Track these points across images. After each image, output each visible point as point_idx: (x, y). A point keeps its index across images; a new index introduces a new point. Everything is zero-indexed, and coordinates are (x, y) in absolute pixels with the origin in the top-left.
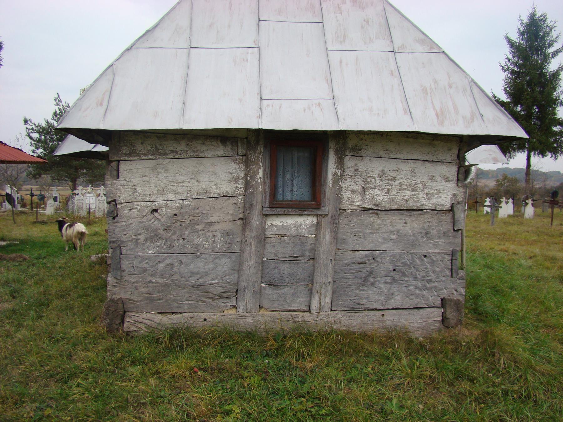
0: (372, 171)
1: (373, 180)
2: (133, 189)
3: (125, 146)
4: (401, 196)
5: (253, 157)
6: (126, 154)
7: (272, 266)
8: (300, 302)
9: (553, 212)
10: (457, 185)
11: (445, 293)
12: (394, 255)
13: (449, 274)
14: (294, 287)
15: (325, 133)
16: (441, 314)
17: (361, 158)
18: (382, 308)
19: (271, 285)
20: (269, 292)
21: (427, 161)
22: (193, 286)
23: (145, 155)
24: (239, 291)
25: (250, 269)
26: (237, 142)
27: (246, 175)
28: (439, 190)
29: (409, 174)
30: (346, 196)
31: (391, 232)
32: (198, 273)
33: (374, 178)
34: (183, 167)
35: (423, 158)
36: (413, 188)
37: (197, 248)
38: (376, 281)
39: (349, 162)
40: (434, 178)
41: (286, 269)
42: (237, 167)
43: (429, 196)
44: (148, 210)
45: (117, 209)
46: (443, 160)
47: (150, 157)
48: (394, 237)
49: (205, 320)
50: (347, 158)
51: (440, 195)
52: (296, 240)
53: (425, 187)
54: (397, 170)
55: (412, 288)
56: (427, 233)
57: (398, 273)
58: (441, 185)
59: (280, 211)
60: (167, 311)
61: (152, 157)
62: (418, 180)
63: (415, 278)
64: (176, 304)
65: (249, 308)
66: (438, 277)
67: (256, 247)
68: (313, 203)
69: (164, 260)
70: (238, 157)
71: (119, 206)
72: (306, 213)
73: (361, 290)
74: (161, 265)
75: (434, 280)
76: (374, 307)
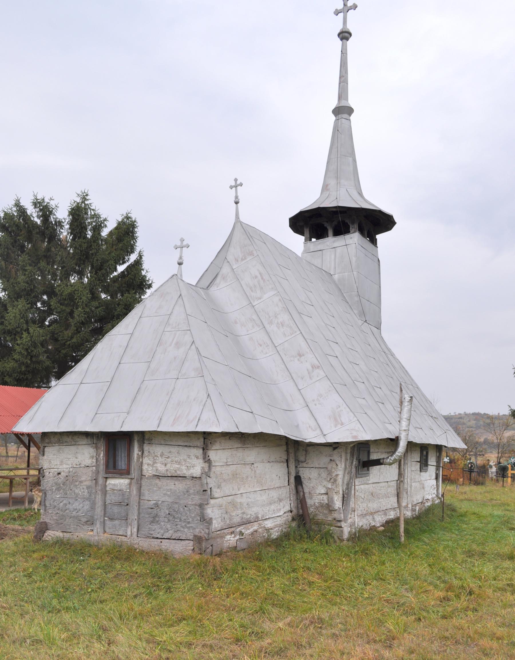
2: (50, 462)
4: (172, 468)
5: (99, 445)
7: (110, 507)
11: (197, 532)
12: (168, 505)
15: (429, 445)
20: (108, 523)
21: (186, 446)
22: (74, 517)
23: (55, 443)
25: (99, 510)
29: (177, 454)
30: (145, 467)
31: (167, 490)
32: (76, 509)
36: (179, 463)
37: (77, 495)
39: (146, 447)
44: (56, 473)
48: (169, 493)
52: (120, 492)
54: (170, 452)
55: (179, 526)
56: (187, 492)
57: (171, 516)
58: (195, 461)
62: (182, 458)
64: (68, 527)
66: (193, 520)
69: (63, 501)
72: (123, 477)
74: (62, 504)
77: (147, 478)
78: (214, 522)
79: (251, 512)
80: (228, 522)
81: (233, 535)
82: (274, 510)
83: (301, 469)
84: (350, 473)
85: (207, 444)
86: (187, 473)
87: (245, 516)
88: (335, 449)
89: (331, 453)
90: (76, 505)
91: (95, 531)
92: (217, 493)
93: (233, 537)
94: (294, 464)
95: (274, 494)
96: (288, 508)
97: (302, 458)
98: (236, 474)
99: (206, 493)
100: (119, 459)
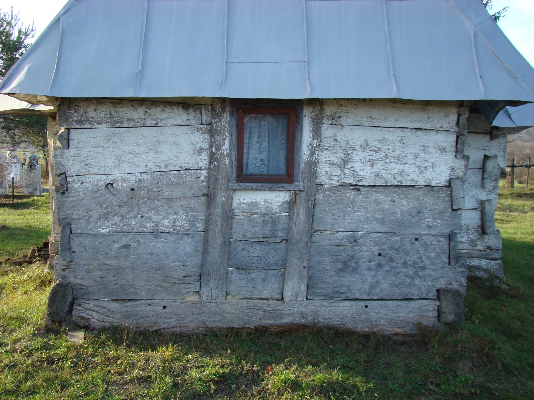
0: (353, 142)
1: (355, 152)
3: (76, 112)
4: (389, 172)
6: (77, 122)
7: (241, 247)
8: (270, 289)
10: (456, 157)
11: (441, 284)
12: (379, 238)
13: (447, 260)
14: (265, 271)
16: (437, 308)
17: (340, 126)
18: (366, 298)
19: (239, 269)
23: (100, 123)
24: (202, 275)
26: (201, 110)
27: (211, 146)
28: (433, 163)
30: (323, 170)
33: (355, 149)
34: (141, 137)
38: (359, 267)
39: (327, 131)
40: (427, 149)
41: (256, 251)
42: (201, 137)
43: (422, 170)
44: (101, 183)
45: (67, 182)
46: (438, 128)
47: (104, 125)
50: (324, 127)
51: (436, 169)
53: (417, 159)
57: (384, 260)
58: (435, 156)
59: (254, 185)
60: (122, 298)
61: (107, 126)
63: (405, 264)
65: (214, 294)
66: (433, 264)
67: (222, 225)
68: (284, 176)
71: (69, 180)
73: (341, 277)
75: (428, 267)
76: (356, 297)
86: (420, 180)
88: (492, 138)
89: (488, 144)
100: (234, 162)
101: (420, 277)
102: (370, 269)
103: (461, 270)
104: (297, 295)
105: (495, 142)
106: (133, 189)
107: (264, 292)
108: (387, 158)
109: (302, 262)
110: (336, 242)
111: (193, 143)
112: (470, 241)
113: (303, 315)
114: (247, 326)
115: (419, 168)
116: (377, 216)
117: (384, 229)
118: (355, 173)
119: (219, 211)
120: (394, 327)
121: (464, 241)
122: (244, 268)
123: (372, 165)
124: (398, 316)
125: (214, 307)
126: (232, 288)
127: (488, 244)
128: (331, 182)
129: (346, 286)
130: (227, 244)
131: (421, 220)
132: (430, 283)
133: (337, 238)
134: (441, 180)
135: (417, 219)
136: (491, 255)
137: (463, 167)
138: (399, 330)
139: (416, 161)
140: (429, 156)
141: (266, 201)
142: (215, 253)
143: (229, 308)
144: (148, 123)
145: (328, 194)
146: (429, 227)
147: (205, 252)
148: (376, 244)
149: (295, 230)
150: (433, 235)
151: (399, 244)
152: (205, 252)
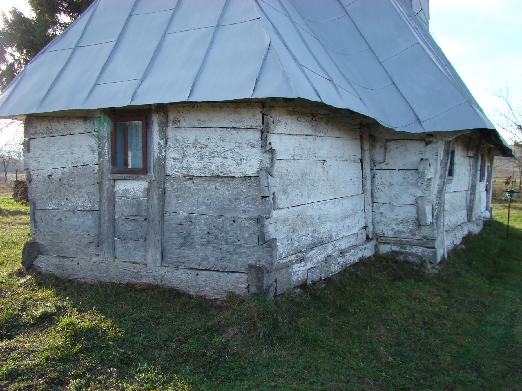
0: (188, 141)
4: (213, 165)
7: (121, 223)
9: (508, 222)
11: (252, 261)
12: (207, 219)
14: (136, 242)
18: (197, 268)
23: (42, 134)
28: (247, 156)
29: (219, 141)
30: (170, 163)
33: (189, 147)
35: (232, 126)
39: (171, 133)
42: (94, 141)
44: (46, 176)
47: (45, 135)
49: (78, 264)
51: (249, 161)
53: (234, 153)
57: (212, 238)
58: (247, 151)
59: (123, 176)
65: (106, 257)
66: (246, 243)
67: (108, 206)
70: (94, 133)
71: (32, 173)
73: (182, 249)
77: (173, 180)
78: (279, 244)
79: (324, 229)
80: (296, 245)
81: (303, 264)
82: (349, 226)
83: (378, 172)
84: (475, 176)
85: (268, 124)
86: (238, 172)
87: (316, 235)
88: (427, 144)
89: (423, 149)
90: (75, 220)
91: (102, 256)
92: (282, 201)
93: (304, 266)
94: (369, 164)
95: (348, 204)
96: (363, 224)
97: (379, 158)
98: (306, 175)
99: (267, 200)
101: (237, 253)
102: (201, 245)
103: (268, 249)
104: (154, 262)
105: (429, 147)
106: (60, 180)
107: (136, 258)
108: (212, 153)
109: (157, 237)
110: (178, 221)
111: (89, 145)
112: (410, 231)
113: (155, 277)
114: (121, 282)
115: (236, 161)
116: (206, 201)
117: (211, 212)
118: (189, 167)
119: (105, 195)
120: (215, 293)
121: (405, 231)
122: (124, 239)
123: (202, 159)
124: (219, 285)
125: (104, 266)
126: (118, 253)
127: (425, 234)
128: (176, 173)
129: (185, 258)
130: (113, 220)
131: (238, 205)
132: (245, 260)
133: (179, 218)
134: (253, 172)
135: (235, 204)
136: (427, 243)
137: (269, 160)
138: (219, 297)
139: (233, 155)
140: (242, 151)
141: (134, 188)
142: (105, 227)
143: (112, 267)
144: (66, 133)
145: (173, 182)
146: (244, 211)
147: (100, 226)
148: (206, 224)
149: (151, 210)
150: (245, 218)
151: (221, 225)
152: (100, 226)
